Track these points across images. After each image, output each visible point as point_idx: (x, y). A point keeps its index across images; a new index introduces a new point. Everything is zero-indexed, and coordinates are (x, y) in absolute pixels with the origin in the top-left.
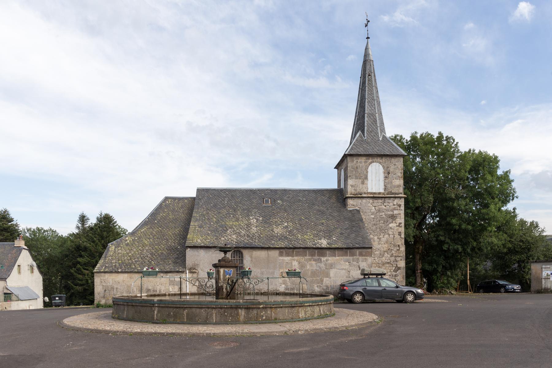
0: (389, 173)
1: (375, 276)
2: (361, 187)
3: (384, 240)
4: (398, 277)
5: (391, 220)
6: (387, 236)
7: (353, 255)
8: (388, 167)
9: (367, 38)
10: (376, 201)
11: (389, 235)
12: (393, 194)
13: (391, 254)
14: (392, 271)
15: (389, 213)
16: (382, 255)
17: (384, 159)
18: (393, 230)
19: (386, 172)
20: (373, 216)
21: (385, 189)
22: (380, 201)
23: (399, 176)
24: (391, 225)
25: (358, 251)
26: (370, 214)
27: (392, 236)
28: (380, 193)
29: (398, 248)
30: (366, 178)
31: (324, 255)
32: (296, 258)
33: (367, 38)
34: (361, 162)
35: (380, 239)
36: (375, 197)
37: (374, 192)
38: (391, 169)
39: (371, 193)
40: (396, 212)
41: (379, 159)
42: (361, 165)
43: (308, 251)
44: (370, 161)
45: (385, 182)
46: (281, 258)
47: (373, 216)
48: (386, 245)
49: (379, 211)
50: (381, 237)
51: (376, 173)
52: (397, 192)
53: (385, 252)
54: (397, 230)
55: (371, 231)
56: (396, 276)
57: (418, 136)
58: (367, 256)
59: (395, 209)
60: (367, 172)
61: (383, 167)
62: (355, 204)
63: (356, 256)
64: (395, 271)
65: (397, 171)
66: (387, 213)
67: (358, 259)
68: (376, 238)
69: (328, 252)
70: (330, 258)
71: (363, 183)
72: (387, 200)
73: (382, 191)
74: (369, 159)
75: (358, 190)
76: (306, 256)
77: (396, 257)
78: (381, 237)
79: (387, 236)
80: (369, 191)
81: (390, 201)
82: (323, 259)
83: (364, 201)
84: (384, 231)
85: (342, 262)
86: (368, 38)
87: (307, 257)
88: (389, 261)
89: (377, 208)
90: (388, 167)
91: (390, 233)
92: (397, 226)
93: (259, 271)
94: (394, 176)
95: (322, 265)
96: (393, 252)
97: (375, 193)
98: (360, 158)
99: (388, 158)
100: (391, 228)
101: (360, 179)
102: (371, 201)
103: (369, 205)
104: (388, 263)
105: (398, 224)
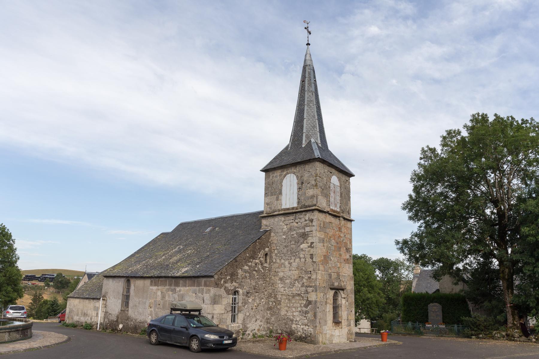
0: (302, 183)
1: (179, 312)
2: (275, 203)
3: (295, 265)
4: (309, 315)
5: (301, 240)
6: (297, 260)
7: (199, 285)
8: (302, 177)
9: (307, 44)
10: (287, 218)
11: (300, 258)
12: (306, 207)
13: (301, 283)
14: (302, 305)
15: (300, 231)
16: (292, 285)
17: (298, 168)
18: (304, 253)
19: (300, 182)
20: (284, 237)
21: (298, 203)
22: (292, 217)
23: (313, 185)
24: (302, 246)
25: (203, 280)
26: (282, 234)
27: (303, 260)
28: (293, 208)
29: (309, 275)
30: (281, 193)
31: (177, 285)
32: (160, 287)
33: (309, 44)
34: (276, 177)
35: (290, 264)
36: (288, 213)
37: (288, 207)
38: (305, 178)
39: (285, 209)
40: (308, 229)
41: (293, 169)
42: (276, 179)
43: (168, 281)
44: (284, 173)
45: (298, 194)
46: (151, 287)
47: (284, 237)
48: (297, 272)
49: (290, 229)
50: (292, 261)
51: (291, 185)
52: (310, 204)
53: (295, 280)
54: (309, 252)
55: (282, 255)
56: (307, 312)
57: (470, 124)
58: (210, 286)
59: (306, 226)
60: (282, 186)
61: (297, 177)
62: (268, 224)
63: (201, 286)
64: (306, 306)
65: (311, 179)
66: (298, 231)
67: (203, 289)
68: (287, 263)
69: (181, 282)
70: (182, 288)
71: (277, 199)
72: (298, 215)
73: (295, 205)
74: (283, 171)
75: (273, 208)
76: (166, 285)
77: (307, 287)
78: (292, 261)
79: (297, 260)
80: (283, 207)
81: (302, 216)
82: (178, 289)
83: (276, 219)
84: (294, 253)
85: (190, 294)
86: (308, 44)
87: (167, 287)
88: (299, 292)
89: (288, 226)
90: (302, 177)
91: (302, 256)
92: (309, 247)
93: (138, 300)
94: (309, 185)
95: (176, 296)
96: (305, 280)
97: (288, 209)
98: (275, 172)
99: (302, 166)
100: (302, 250)
101: (275, 195)
102: (283, 219)
103: (281, 223)
104: (299, 295)
105: (309, 245)
